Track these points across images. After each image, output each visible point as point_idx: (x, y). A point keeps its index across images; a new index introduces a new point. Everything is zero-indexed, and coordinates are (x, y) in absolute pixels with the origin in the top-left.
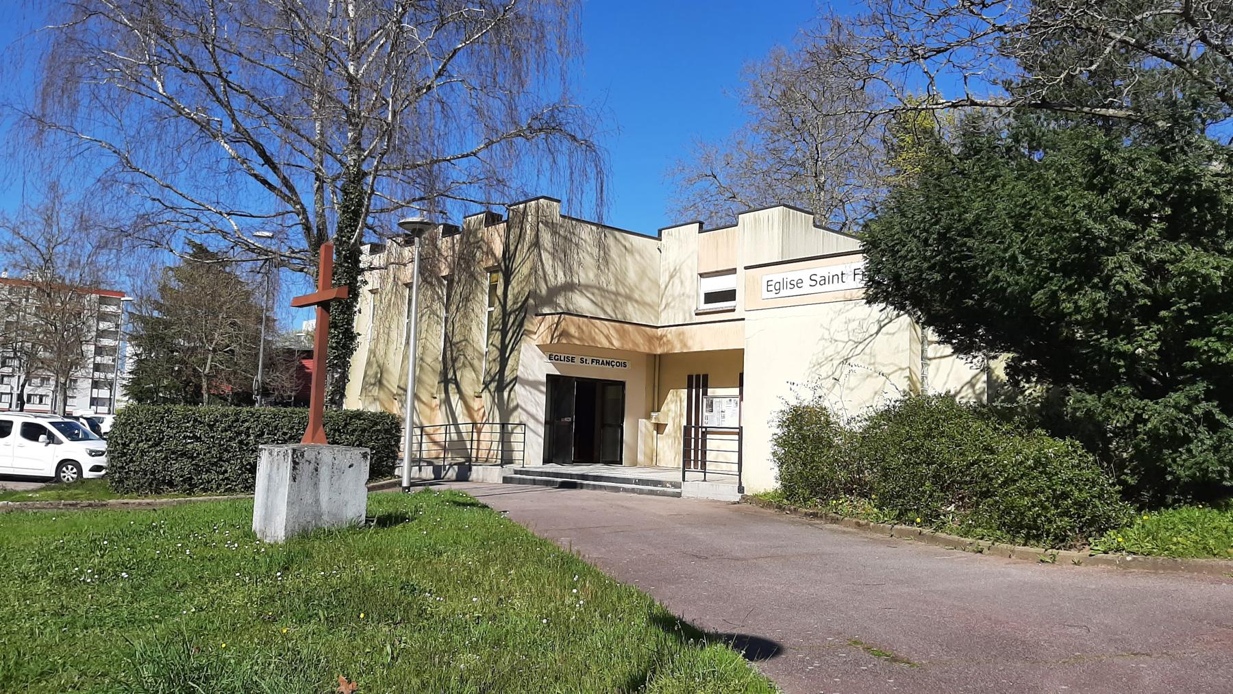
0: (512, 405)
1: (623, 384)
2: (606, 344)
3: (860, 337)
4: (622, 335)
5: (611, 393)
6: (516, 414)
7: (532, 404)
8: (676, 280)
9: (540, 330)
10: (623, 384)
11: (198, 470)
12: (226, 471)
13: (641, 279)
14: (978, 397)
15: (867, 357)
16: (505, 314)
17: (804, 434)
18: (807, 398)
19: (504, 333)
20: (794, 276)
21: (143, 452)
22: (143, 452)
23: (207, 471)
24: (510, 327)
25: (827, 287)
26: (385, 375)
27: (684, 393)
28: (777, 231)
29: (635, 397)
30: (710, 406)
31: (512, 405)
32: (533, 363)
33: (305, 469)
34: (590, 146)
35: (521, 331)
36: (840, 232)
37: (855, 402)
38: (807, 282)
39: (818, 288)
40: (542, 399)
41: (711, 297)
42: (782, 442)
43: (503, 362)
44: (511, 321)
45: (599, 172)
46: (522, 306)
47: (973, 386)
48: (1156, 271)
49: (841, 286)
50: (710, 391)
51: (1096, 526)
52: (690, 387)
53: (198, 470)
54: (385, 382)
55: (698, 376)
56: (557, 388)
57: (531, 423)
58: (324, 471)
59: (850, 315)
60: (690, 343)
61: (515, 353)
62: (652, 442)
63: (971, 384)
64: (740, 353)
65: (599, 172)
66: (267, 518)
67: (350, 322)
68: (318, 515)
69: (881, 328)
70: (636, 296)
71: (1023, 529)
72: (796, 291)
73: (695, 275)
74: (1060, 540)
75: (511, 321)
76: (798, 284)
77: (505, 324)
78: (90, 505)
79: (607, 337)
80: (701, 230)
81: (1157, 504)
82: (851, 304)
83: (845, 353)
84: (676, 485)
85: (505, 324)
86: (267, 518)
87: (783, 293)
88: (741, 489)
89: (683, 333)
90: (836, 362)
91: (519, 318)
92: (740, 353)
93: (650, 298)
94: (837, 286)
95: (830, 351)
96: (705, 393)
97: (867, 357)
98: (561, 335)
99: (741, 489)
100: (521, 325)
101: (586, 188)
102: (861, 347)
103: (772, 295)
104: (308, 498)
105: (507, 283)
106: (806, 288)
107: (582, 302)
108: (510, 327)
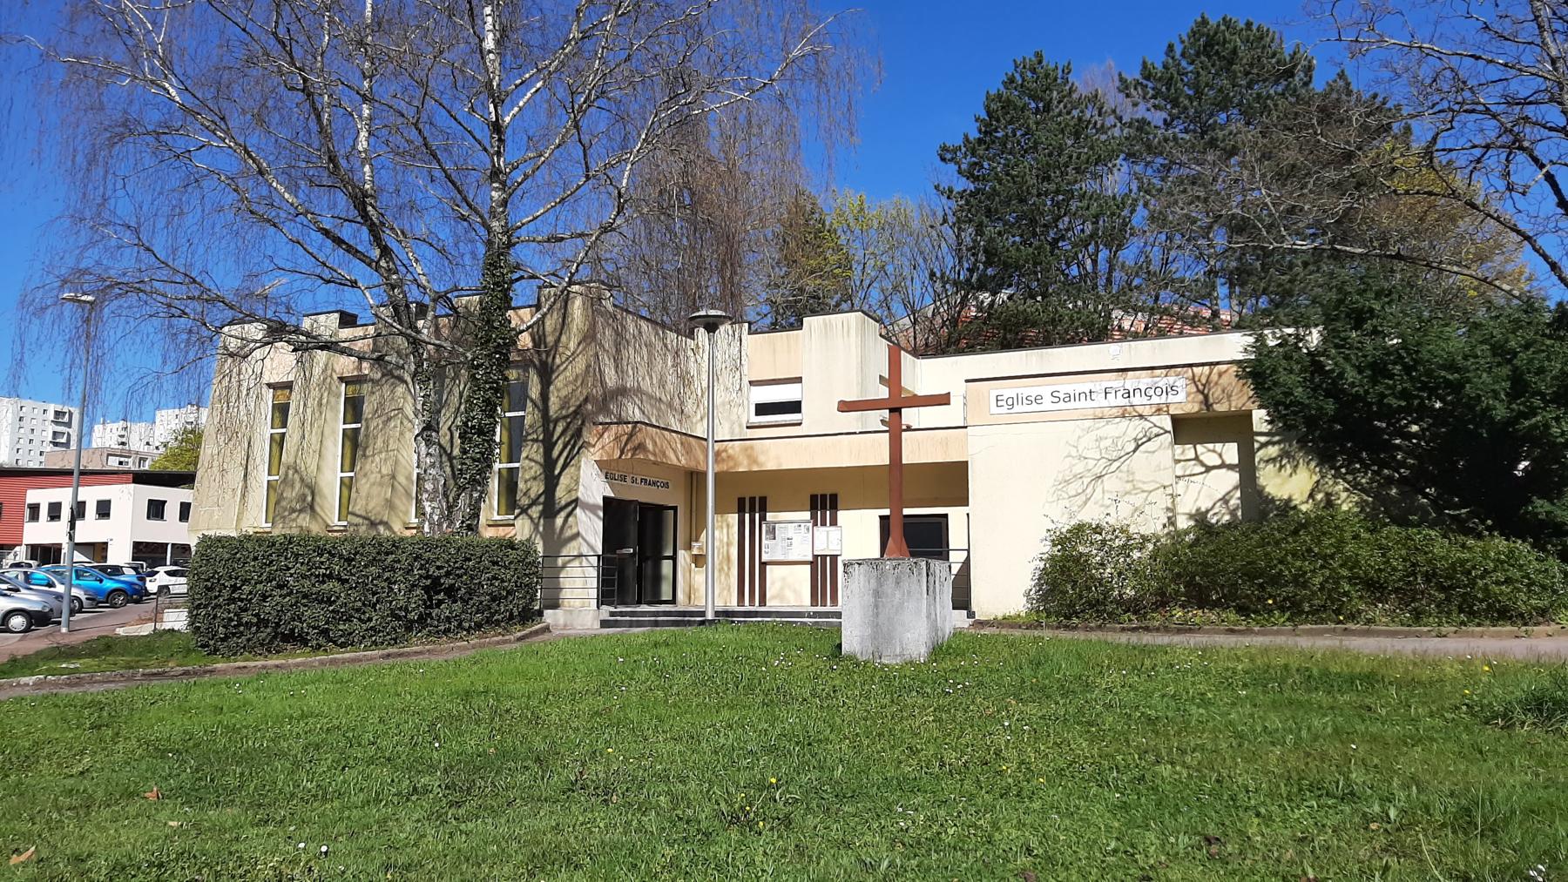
0: (568, 533)
2: (675, 462)
3: (1115, 455)
4: (688, 450)
6: (574, 544)
9: (600, 446)
12: (370, 619)
14: (1233, 513)
15: (1124, 475)
20: (1034, 392)
21: (264, 597)
23: (349, 620)
25: (1072, 405)
26: (317, 499)
27: (734, 518)
28: (854, 338)
30: (772, 533)
31: (568, 533)
35: (576, 444)
36: (774, 330)
38: (1048, 399)
39: (1062, 405)
41: (762, 409)
44: (559, 429)
46: (576, 413)
47: (1226, 502)
49: (1089, 404)
50: (770, 516)
52: (741, 511)
54: (318, 509)
55: (752, 500)
56: (613, 510)
59: (1101, 433)
60: (762, 458)
61: (570, 470)
63: (1225, 500)
64: (963, 466)
69: (1138, 446)
72: (1034, 407)
75: (559, 429)
76: (1038, 399)
78: (186, 673)
82: (1102, 422)
83: (1097, 471)
85: (548, 434)
87: (1017, 408)
89: (752, 448)
90: (1086, 481)
91: (573, 427)
92: (963, 466)
94: (1083, 403)
95: (1079, 468)
96: (763, 518)
97: (1124, 475)
98: (635, 449)
100: (578, 434)
102: (1116, 464)
103: (1004, 410)
105: (546, 382)
106: (1047, 404)
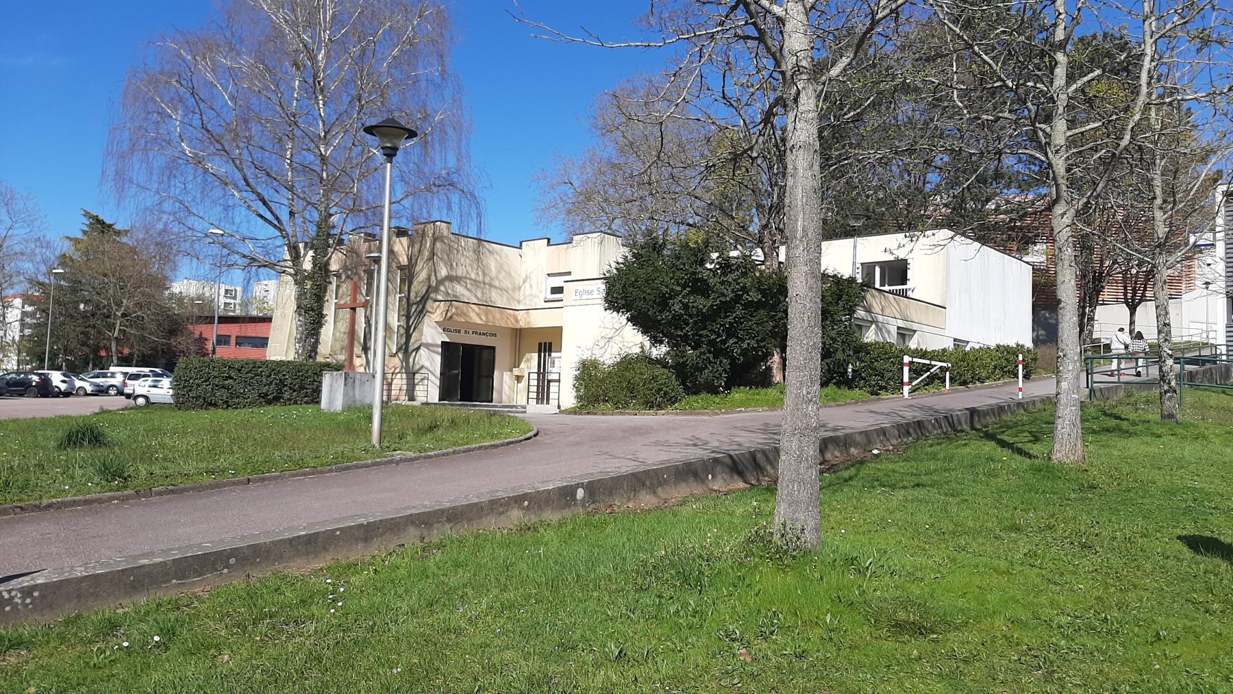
1: (493, 348)
2: (479, 321)
5: (485, 354)
7: (431, 362)
8: (527, 285)
9: (436, 313)
10: (493, 348)
11: (232, 396)
13: (499, 272)
16: (409, 305)
17: (588, 372)
18: (587, 355)
19: (408, 317)
20: (590, 288)
22: (198, 385)
24: (413, 311)
29: (502, 357)
32: (431, 333)
33: (350, 381)
34: (472, 195)
35: (422, 313)
37: (608, 357)
40: (438, 359)
42: (577, 378)
43: (408, 337)
45: (479, 215)
48: (686, 307)
51: (673, 401)
53: (232, 396)
57: (431, 376)
58: (357, 382)
62: (511, 387)
65: (479, 215)
66: (331, 402)
67: (321, 307)
68: (355, 401)
70: (497, 284)
71: (650, 405)
73: (545, 275)
74: (660, 407)
77: (409, 311)
79: (475, 316)
80: (549, 244)
81: (696, 393)
84: (524, 407)
86: (331, 402)
88: (559, 407)
93: (507, 284)
99: (559, 407)
101: (471, 225)
104: (351, 394)
107: (459, 289)
108: (413, 311)
